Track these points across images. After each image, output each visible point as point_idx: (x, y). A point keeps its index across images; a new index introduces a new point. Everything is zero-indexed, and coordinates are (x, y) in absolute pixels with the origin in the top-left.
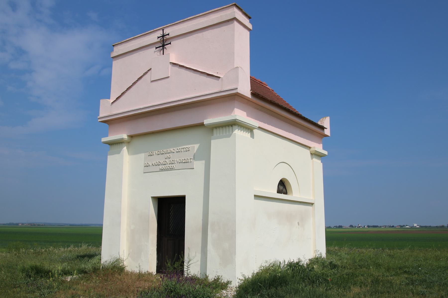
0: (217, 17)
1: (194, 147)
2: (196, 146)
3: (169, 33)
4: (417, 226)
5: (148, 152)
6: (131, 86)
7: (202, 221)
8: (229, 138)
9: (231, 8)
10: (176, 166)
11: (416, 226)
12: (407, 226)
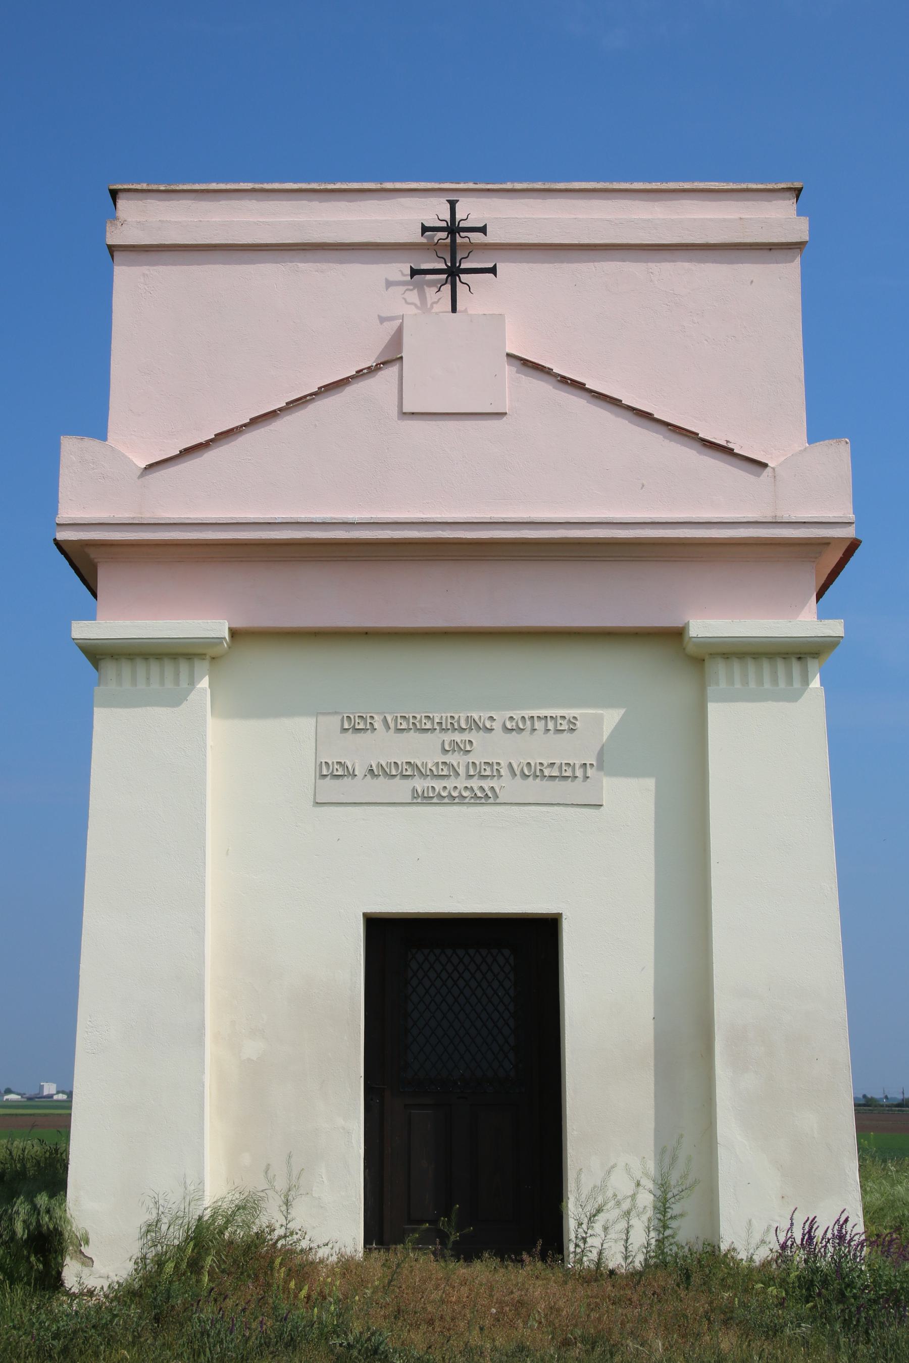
0: (725, 220)
1: (599, 719)
2: (611, 718)
3: (485, 226)
4: (58, 1092)
5: (336, 713)
6: (280, 409)
7: (652, 1022)
8: (793, 704)
9: (784, 199)
10: (507, 787)
11: (51, 1096)
12: (8, 1091)
